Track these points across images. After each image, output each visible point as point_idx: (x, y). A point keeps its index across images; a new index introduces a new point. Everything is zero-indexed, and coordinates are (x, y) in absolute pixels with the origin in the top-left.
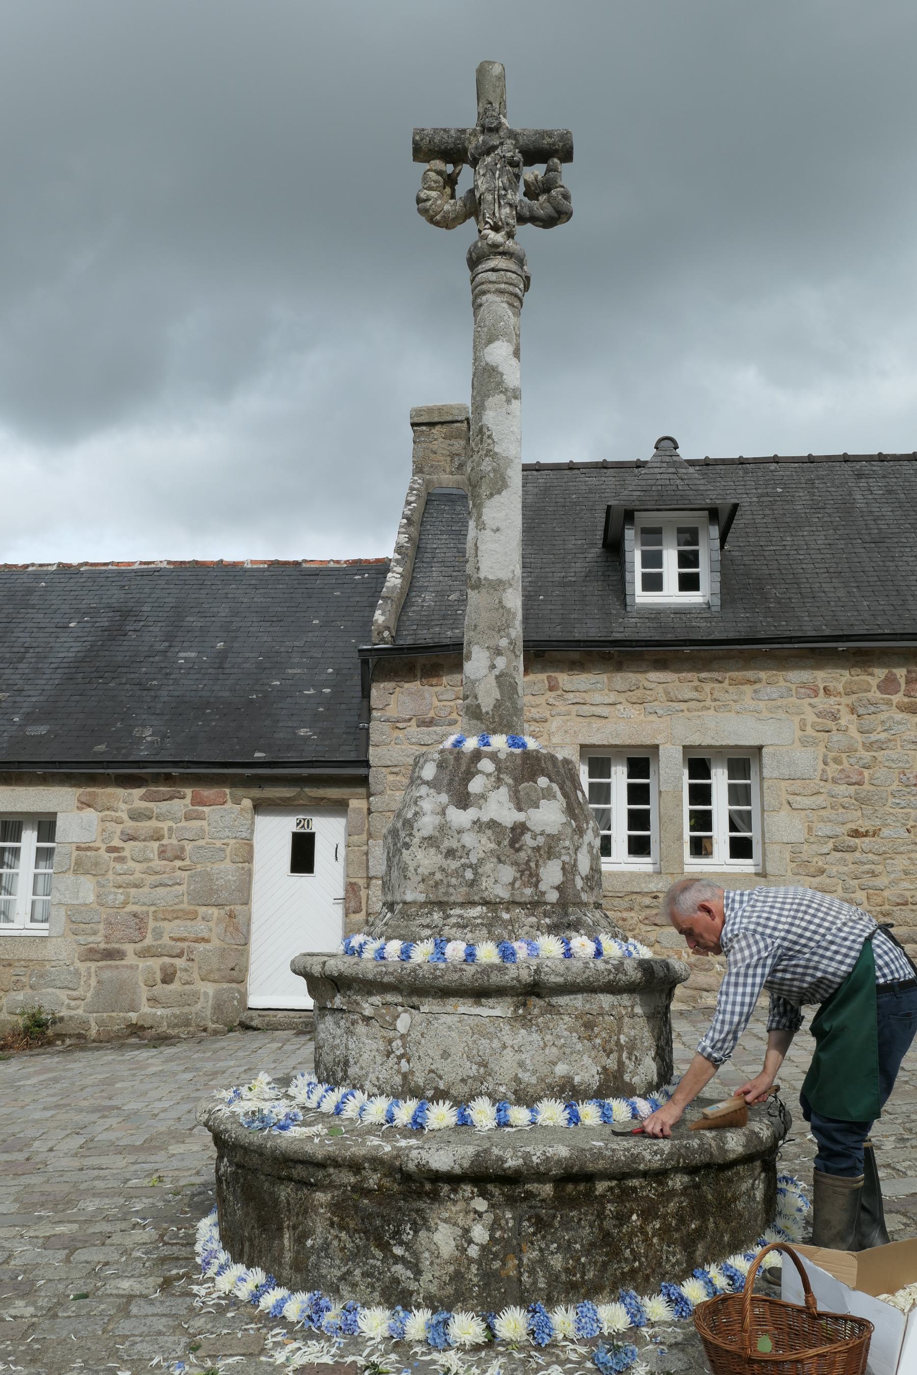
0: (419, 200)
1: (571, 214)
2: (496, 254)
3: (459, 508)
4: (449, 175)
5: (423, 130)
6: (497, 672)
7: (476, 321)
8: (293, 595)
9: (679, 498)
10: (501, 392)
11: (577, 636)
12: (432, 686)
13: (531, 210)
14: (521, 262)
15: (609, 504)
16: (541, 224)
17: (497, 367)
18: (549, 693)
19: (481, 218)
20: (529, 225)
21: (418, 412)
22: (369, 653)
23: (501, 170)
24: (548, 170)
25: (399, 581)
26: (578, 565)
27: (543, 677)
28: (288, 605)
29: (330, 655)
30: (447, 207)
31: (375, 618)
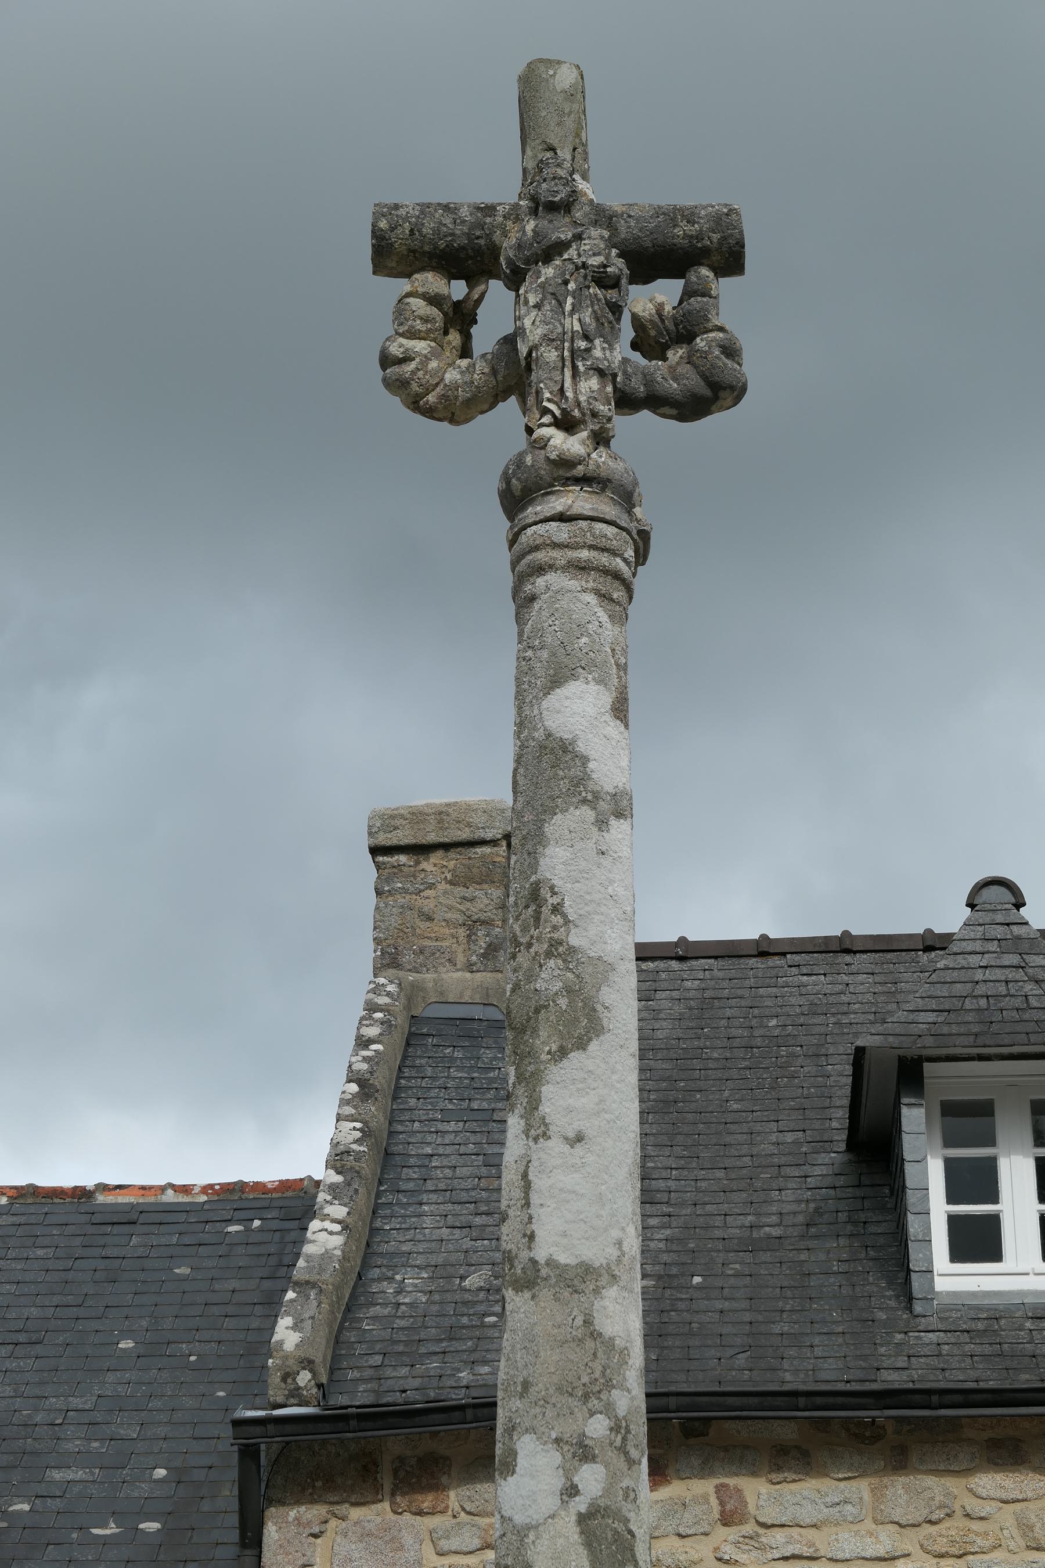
0: (386, 361)
1: (743, 390)
2: (568, 481)
3: (489, 1054)
4: (457, 305)
5: (396, 207)
6: (580, 1504)
7: (521, 634)
8: (70, 1276)
9: (1031, 1027)
10: (584, 801)
11: (791, 1380)
12: (420, 1513)
13: (648, 380)
14: (627, 498)
15: (860, 1043)
16: (674, 412)
17: (573, 742)
18: (722, 1532)
19: (531, 400)
20: (645, 414)
21: (387, 820)
22: (258, 1430)
23: (577, 294)
24: (688, 294)
25: (338, 1241)
26: (788, 1195)
27: (704, 1487)
28: (56, 1300)
29: (161, 1431)
30: (451, 376)
31: (276, 1338)
